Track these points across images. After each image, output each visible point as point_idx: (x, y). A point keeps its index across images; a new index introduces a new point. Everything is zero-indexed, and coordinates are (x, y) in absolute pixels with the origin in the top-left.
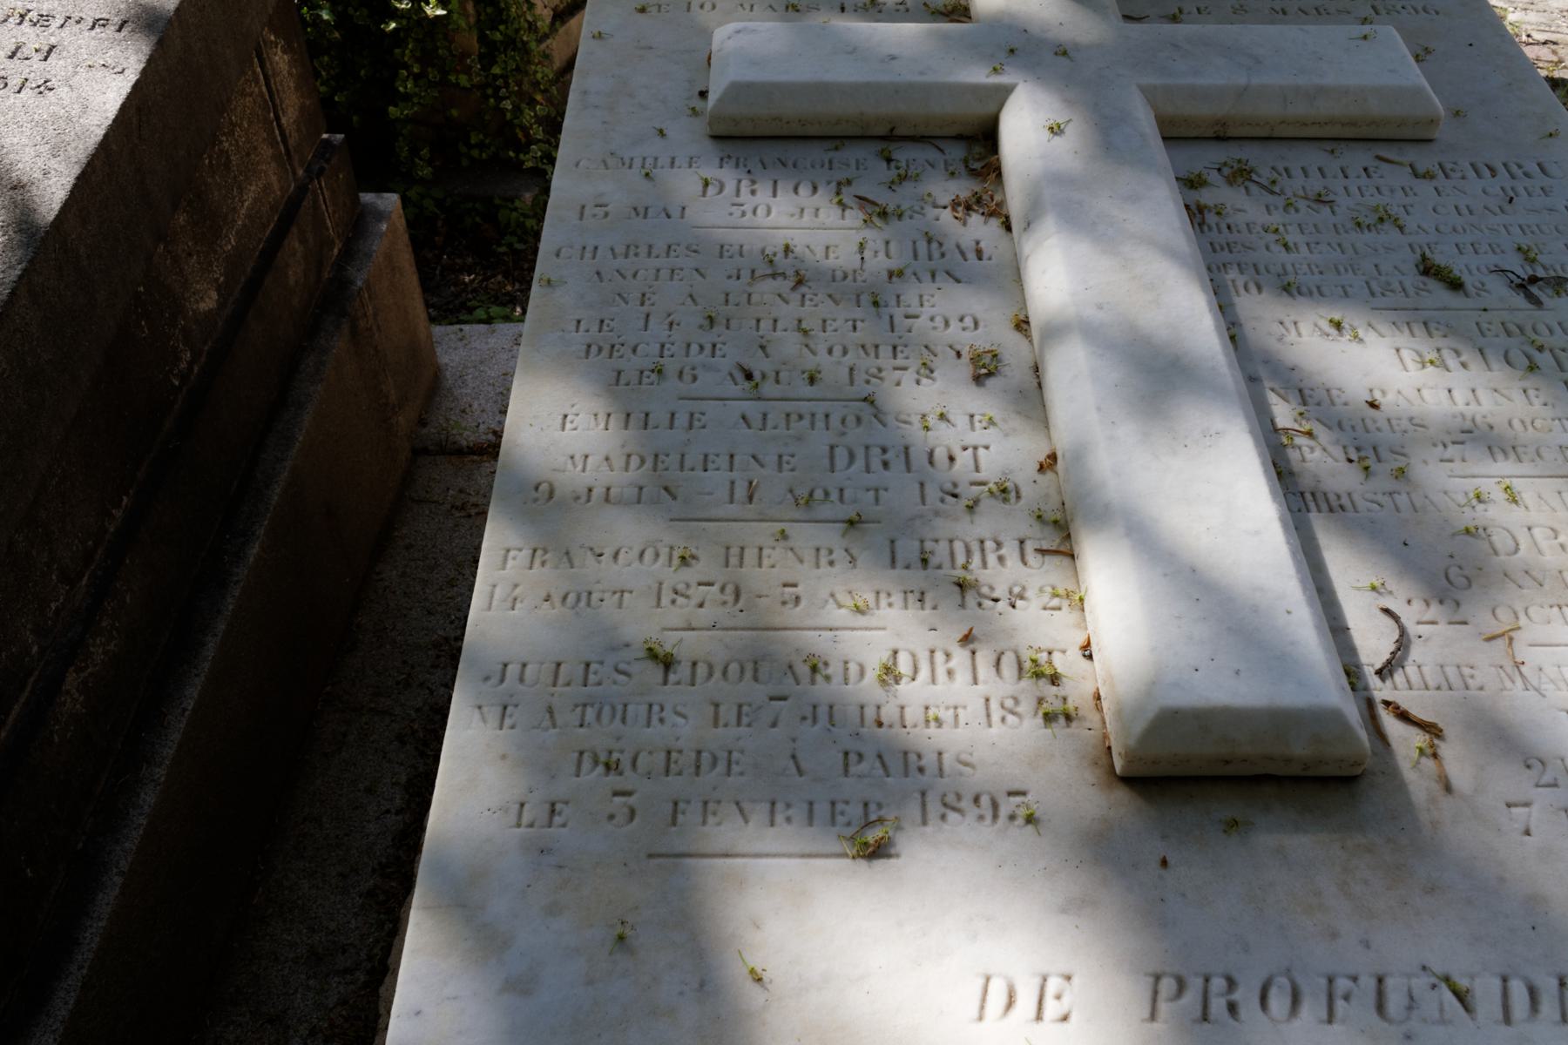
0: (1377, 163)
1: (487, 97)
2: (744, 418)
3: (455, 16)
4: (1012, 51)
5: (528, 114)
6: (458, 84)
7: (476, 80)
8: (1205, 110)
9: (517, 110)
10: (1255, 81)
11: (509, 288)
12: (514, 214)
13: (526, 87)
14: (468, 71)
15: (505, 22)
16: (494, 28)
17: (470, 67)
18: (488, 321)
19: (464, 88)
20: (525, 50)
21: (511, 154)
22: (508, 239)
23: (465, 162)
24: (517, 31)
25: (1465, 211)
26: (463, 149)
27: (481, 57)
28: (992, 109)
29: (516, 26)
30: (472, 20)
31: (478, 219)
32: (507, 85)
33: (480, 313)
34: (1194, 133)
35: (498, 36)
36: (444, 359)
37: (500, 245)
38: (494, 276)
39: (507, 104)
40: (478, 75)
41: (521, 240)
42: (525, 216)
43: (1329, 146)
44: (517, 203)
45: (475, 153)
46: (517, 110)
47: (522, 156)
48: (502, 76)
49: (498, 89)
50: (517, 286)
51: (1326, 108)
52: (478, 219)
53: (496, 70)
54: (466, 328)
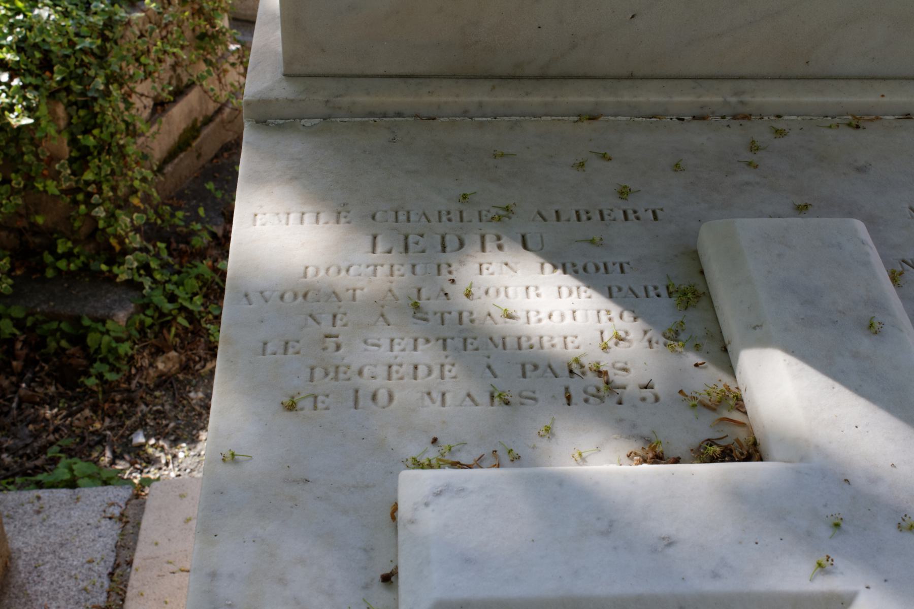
1: (76, 203)
3: (43, 123)
4: (837, 525)
5: (124, 220)
6: (45, 192)
7: (65, 185)
9: (112, 217)
11: (98, 425)
12: (106, 339)
13: (122, 191)
14: (56, 176)
15: (100, 126)
16: (87, 132)
17: (59, 173)
18: (72, 484)
19: (53, 196)
20: (122, 154)
21: (104, 267)
22: (98, 367)
23: (50, 273)
24: (112, 135)
26: (48, 258)
27: (72, 161)
29: (112, 129)
30: (63, 123)
31: (64, 343)
32: (100, 191)
33: (61, 472)
35: (90, 141)
36: (17, 542)
37: (89, 376)
38: (81, 410)
39: (100, 212)
40: (67, 179)
41: (114, 369)
42: (119, 340)
44: (109, 325)
45: (62, 264)
46: (112, 217)
47: (115, 269)
48: (94, 182)
49: (89, 195)
50: (107, 421)
52: (64, 343)
53: (89, 176)
54: (44, 493)
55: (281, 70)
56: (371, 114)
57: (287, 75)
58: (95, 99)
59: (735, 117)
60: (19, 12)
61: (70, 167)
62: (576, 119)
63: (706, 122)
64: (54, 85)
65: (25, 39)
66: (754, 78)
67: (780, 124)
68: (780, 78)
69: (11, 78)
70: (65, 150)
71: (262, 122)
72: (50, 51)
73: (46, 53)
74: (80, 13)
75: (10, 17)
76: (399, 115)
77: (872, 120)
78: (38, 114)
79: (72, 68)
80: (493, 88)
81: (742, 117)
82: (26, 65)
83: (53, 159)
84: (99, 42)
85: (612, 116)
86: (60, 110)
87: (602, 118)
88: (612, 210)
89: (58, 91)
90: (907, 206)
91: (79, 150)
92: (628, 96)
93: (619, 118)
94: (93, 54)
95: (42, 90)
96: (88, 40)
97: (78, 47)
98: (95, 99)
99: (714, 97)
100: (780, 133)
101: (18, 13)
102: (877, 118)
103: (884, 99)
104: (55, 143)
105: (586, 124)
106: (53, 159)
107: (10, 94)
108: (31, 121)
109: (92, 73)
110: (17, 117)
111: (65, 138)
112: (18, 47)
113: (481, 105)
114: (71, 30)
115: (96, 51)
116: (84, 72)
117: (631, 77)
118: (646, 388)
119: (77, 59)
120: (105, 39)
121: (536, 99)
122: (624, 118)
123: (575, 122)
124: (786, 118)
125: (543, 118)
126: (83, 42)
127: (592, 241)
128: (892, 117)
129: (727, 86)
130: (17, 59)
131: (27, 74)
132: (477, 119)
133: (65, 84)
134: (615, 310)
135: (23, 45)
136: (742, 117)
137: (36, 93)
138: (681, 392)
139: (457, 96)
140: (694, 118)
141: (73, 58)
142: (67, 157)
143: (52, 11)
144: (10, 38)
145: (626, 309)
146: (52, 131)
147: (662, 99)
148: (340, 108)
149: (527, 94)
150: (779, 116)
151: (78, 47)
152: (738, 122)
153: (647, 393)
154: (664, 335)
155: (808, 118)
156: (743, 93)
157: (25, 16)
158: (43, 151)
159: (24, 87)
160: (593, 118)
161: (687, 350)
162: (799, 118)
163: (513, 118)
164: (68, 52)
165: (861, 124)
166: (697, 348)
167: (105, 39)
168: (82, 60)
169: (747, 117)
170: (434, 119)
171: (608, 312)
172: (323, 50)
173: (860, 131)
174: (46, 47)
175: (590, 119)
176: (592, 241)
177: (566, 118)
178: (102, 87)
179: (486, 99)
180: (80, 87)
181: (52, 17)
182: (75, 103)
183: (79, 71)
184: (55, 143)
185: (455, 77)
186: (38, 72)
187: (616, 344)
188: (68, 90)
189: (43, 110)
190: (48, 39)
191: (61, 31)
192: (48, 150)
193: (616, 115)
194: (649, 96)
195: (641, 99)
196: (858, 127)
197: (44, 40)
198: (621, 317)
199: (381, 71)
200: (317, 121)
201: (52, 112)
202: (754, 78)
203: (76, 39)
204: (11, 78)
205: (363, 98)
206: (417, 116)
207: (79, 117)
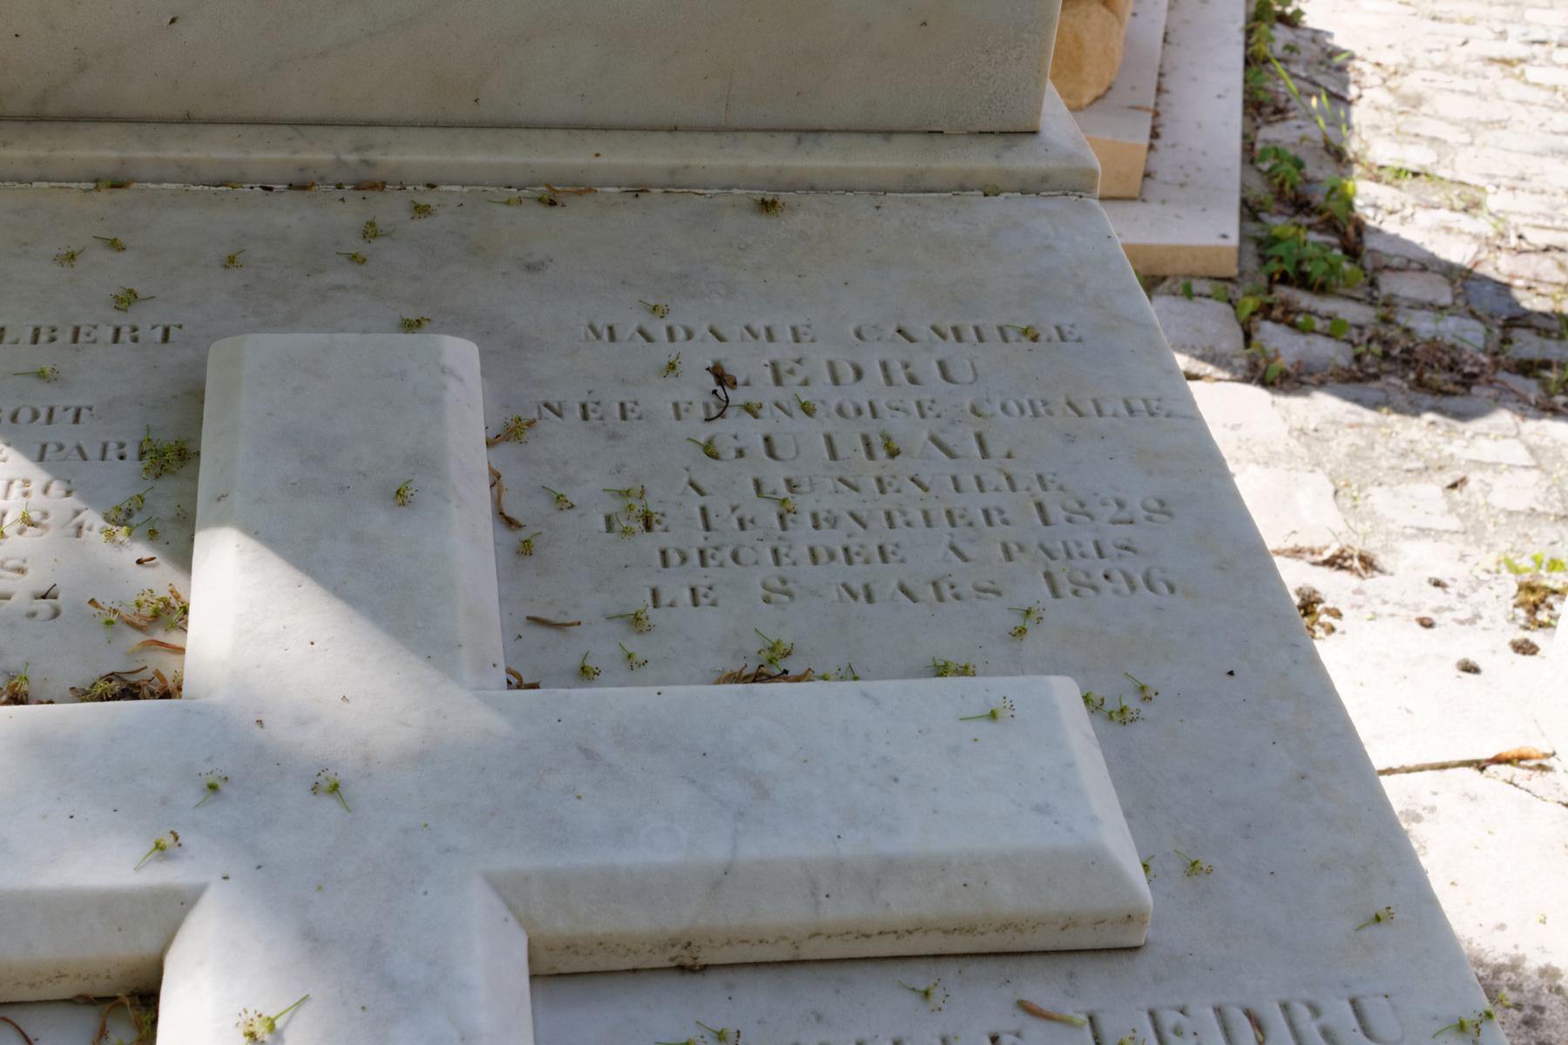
0: (1023, 1019)
2: (903, 589)
4: (213, 788)
8: (640, 922)
10: (750, 850)
25: (900, 376)
28: (145, 945)
34: (628, 963)
43: (920, 976)
51: (902, 904)
59: (358, 187)
66: (393, 124)
67: (426, 198)
68: (436, 125)
77: (580, 193)
81: (370, 186)
85: (153, 182)
87: (135, 185)
88: (95, 327)
90: (586, 322)
92: (176, 149)
93: (165, 185)
99: (318, 153)
100: (421, 210)
102: (589, 190)
103: (602, 160)
105: (105, 196)
117: (188, 120)
118: (44, 597)
122: (173, 186)
124: (444, 188)
125: (35, 184)
127: (41, 375)
129: (346, 137)
134: (39, 477)
136: (370, 186)
138: (92, 601)
140: (291, 186)
145: (57, 478)
147: (233, 155)
150: (431, 186)
152: (360, 194)
153: (44, 606)
154: (107, 518)
155: (480, 188)
156: (371, 147)
160: (117, 185)
161: (134, 540)
162: (466, 189)
165: (560, 199)
166: (153, 535)
169: (379, 186)
171: (26, 482)
175: (113, 186)
176: (41, 375)
177: (74, 185)
187: (21, 532)
193: (159, 181)
194: (212, 150)
195: (196, 155)
196: (552, 203)
198: (46, 491)
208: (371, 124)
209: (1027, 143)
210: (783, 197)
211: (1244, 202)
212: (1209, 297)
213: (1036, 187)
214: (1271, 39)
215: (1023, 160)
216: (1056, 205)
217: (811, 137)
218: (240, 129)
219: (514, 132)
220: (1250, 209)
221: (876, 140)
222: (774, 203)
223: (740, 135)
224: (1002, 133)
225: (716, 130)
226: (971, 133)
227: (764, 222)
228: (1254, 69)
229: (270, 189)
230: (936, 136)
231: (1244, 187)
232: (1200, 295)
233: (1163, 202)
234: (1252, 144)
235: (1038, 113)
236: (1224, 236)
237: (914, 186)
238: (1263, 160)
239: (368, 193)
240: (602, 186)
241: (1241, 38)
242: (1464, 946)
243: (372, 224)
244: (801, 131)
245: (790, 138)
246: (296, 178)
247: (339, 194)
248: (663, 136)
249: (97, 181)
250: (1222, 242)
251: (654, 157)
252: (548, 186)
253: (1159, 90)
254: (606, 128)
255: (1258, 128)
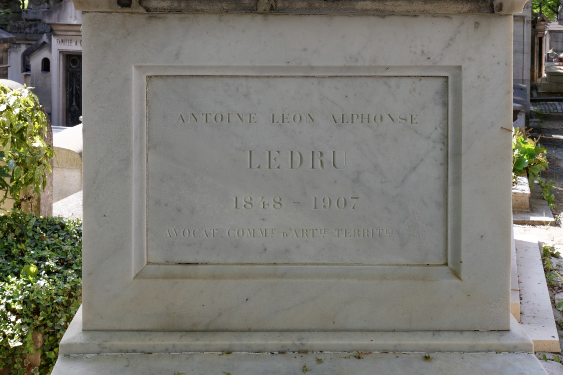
30: (39, 345)
55: (81, 328)
56: (121, 351)
57: (83, 330)
58: (59, 330)
59: (300, 352)
60: (29, 282)
61: (39, 371)
62: (221, 353)
63: (284, 355)
64: (38, 323)
65: (28, 297)
66: (309, 331)
67: (321, 356)
68: (322, 331)
69: (17, 319)
70: (39, 361)
71: (67, 356)
72: (39, 304)
73: (38, 305)
74: (61, 282)
75: (24, 285)
76: (134, 351)
77: (367, 354)
78: (26, 340)
79: (49, 313)
80: (182, 336)
81: (303, 352)
82: (26, 312)
83: (31, 366)
84: (67, 298)
86: (40, 337)
87: (234, 353)
89: (40, 326)
91: (46, 360)
93: (243, 353)
94: (63, 305)
95: (31, 326)
96: (61, 297)
97: (55, 301)
98: (59, 330)
99: (288, 341)
100: (319, 361)
101: (29, 283)
102: (370, 353)
103: (373, 342)
104: (33, 357)
105: (225, 357)
106: (31, 366)
107: (14, 328)
108: (21, 344)
109: (59, 316)
110: (15, 341)
111: (40, 353)
112: (24, 302)
113: (174, 346)
114: (53, 292)
115: (65, 303)
116: (55, 315)
117: (249, 330)
119: (53, 308)
120: (70, 296)
121: (202, 342)
123: (220, 355)
124: (325, 352)
126: (58, 298)
128: (378, 352)
129: (296, 335)
130: (22, 308)
131: (25, 317)
132: (172, 353)
133: (44, 322)
135: (27, 300)
136: (303, 352)
137: (27, 327)
139: (163, 341)
141: (51, 307)
142: (39, 365)
143: (47, 281)
144: (20, 297)
146: (32, 350)
148: (106, 348)
149: (197, 340)
151: (55, 301)
152: (300, 355)
156: (303, 339)
157: (32, 284)
158: (26, 361)
159: (22, 324)
160: (229, 353)
162: (332, 353)
163: (190, 353)
164: (50, 304)
165: (361, 356)
167: (70, 296)
168: (56, 309)
169: (306, 352)
170: (151, 353)
172: (102, 318)
173: (360, 360)
174: (38, 302)
178: (63, 324)
179: (177, 343)
180: (51, 324)
181: (46, 285)
182: (48, 333)
183: (53, 315)
184: (33, 357)
185: (164, 331)
186: (31, 315)
188: (45, 326)
189: (30, 337)
190: (40, 297)
191: (48, 293)
192: (29, 360)
193: (241, 351)
194: (257, 341)
195: (253, 342)
196: (359, 358)
197: (38, 298)
199: (128, 328)
200: (93, 355)
201: (35, 339)
202: (309, 331)
203: (54, 297)
204: (17, 319)
205: (118, 342)
206: (143, 352)
207: (49, 341)
208: (302, 331)
209: (507, 334)
210: (432, 355)
211: (556, 322)
212: (553, 360)
213: (513, 350)
214: (552, 263)
215: (506, 341)
216: (520, 357)
217: (438, 333)
218: (264, 333)
219: (345, 332)
220: (559, 325)
221: (458, 334)
222: (429, 357)
223: (415, 332)
224: (498, 331)
225: (407, 331)
226: (488, 331)
227: (426, 364)
228: (548, 274)
229: (273, 353)
230: (477, 332)
231: (556, 317)
232: (549, 360)
233: (529, 324)
234: (554, 301)
235: (509, 324)
236: (553, 337)
237: (473, 350)
238: (559, 307)
239: (303, 355)
240: (374, 351)
241: (541, 262)
242: (74, 341)
243: (305, 366)
244: (434, 331)
245: (430, 334)
246: (281, 349)
247: (294, 355)
248: (391, 333)
249: (223, 351)
250: (553, 339)
251: (389, 341)
252: (357, 351)
253: (519, 282)
254: (373, 331)
255: (554, 295)
